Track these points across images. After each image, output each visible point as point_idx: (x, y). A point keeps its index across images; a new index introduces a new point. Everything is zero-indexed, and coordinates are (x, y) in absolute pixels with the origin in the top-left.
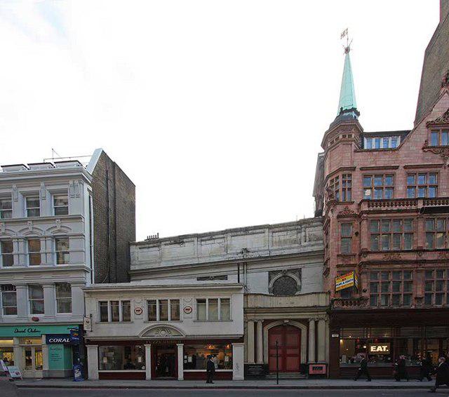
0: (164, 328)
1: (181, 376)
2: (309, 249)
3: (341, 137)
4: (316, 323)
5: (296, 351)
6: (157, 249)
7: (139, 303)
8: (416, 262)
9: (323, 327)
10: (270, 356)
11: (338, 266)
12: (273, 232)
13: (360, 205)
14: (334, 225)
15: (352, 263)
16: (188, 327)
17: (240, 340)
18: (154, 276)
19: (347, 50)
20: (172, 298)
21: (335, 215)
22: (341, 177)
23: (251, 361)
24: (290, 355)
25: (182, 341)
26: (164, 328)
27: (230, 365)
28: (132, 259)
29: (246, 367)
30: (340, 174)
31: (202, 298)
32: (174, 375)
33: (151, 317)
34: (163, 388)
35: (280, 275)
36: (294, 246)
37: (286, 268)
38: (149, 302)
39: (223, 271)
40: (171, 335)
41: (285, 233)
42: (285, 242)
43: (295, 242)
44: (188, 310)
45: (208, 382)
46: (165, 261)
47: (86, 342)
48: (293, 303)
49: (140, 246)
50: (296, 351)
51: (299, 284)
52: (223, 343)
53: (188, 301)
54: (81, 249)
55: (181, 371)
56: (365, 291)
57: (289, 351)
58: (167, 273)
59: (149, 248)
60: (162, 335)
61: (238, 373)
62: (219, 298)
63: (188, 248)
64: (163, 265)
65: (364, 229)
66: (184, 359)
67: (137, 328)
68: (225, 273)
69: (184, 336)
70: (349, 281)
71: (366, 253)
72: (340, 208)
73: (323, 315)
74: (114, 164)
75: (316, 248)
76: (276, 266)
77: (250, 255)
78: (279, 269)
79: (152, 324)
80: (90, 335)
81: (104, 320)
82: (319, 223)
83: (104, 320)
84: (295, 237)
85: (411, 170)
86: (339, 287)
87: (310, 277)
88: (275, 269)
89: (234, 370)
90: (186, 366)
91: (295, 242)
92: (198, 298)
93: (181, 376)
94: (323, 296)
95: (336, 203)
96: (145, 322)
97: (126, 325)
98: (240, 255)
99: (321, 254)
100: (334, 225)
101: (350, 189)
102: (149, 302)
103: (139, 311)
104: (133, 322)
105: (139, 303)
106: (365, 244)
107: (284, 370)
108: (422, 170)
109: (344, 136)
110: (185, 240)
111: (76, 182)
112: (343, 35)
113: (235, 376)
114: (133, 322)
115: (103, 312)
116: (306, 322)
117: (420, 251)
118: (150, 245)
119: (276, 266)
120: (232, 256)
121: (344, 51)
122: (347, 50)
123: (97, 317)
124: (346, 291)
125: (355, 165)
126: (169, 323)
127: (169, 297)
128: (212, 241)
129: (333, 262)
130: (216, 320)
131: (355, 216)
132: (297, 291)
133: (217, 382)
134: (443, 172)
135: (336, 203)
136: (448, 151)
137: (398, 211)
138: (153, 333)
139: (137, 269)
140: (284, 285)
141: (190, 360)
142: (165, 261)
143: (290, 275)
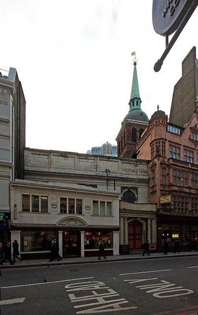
0: (72, 220)
1: (83, 254)
2: (141, 177)
3: (161, 121)
4: (151, 221)
5: (140, 237)
6: (46, 157)
7: (54, 200)
8: (189, 193)
9: (154, 222)
10: (129, 240)
11: (161, 190)
12: (123, 163)
13: (168, 160)
14: (158, 169)
15: (166, 189)
16: (89, 219)
17: (118, 229)
18: (33, 177)
19: (135, 64)
20: (101, 200)
21: (159, 162)
22: (161, 143)
23: (122, 243)
24: (137, 239)
25: (86, 230)
26: (72, 220)
27: (111, 246)
28: (25, 161)
29: (120, 246)
30: (161, 141)
31: (96, 200)
32: (79, 255)
33: (63, 211)
34: (81, 263)
35: (127, 190)
36: (133, 173)
37: (131, 186)
38: (62, 199)
39: (94, 182)
40: (77, 225)
41: (129, 165)
42: (129, 170)
43: (133, 171)
44: (88, 207)
45: (165, 254)
46: (53, 168)
47: (10, 228)
48: (139, 208)
49: (32, 152)
50: (140, 237)
51: (136, 196)
52: (107, 231)
53: (87, 202)
54: (7, 148)
55: (83, 250)
56: (172, 205)
57: (137, 237)
58: (56, 177)
59: (40, 155)
60: (72, 224)
61: (116, 251)
62: (106, 201)
63: (70, 161)
64: (52, 170)
65: (171, 173)
66: (85, 242)
67: (53, 218)
68: (95, 184)
69: (87, 226)
70: (168, 199)
71: (171, 185)
72: (161, 159)
73: (154, 216)
74: (20, 82)
75: (145, 177)
76: (125, 184)
77: (111, 175)
78: (127, 186)
79: (64, 216)
80: (14, 222)
81: (25, 210)
82: (146, 163)
83: (25, 210)
84: (133, 168)
85: (171, 144)
86: (162, 202)
87: (142, 193)
88: (125, 186)
89: (114, 249)
90: (86, 247)
91: (133, 171)
92: (61, 197)
93: (83, 254)
94: (154, 206)
95: (160, 156)
96: (92, 216)
97: (45, 215)
98: (105, 173)
99: (147, 181)
100: (158, 169)
101: (165, 150)
102: (62, 199)
103: (54, 205)
104: (84, 215)
105: (54, 200)
106: (172, 181)
107: (135, 248)
108: (174, 145)
109: (156, 123)
110: (68, 155)
111: (5, 91)
112: (133, 54)
113: (115, 253)
114: (84, 215)
115: (63, 206)
116: (146, 220)
117: (190, 188)
118: (41, 153)
119: (125, 184)
120: (100, 173)
121: (133, 63)
122: (135, 64)
123: (20, 208)
124: (164, 205)
125: (166, 138)
126: (76, 215)
127: (76, 197)
128: (87, 160)
129: (158, 188)
130: (104, 216)
131: (166, 165)
132: (135, 200)
133: (152, 254)
134: (195, 152)
135: (160, 156)
136: (196, 143)
137: (183, 167)
138: (65, 223)
139: (30, 169)
140: (129, 196)
141: (88, 243)
142: (53, 168)
143: (132, 190)
